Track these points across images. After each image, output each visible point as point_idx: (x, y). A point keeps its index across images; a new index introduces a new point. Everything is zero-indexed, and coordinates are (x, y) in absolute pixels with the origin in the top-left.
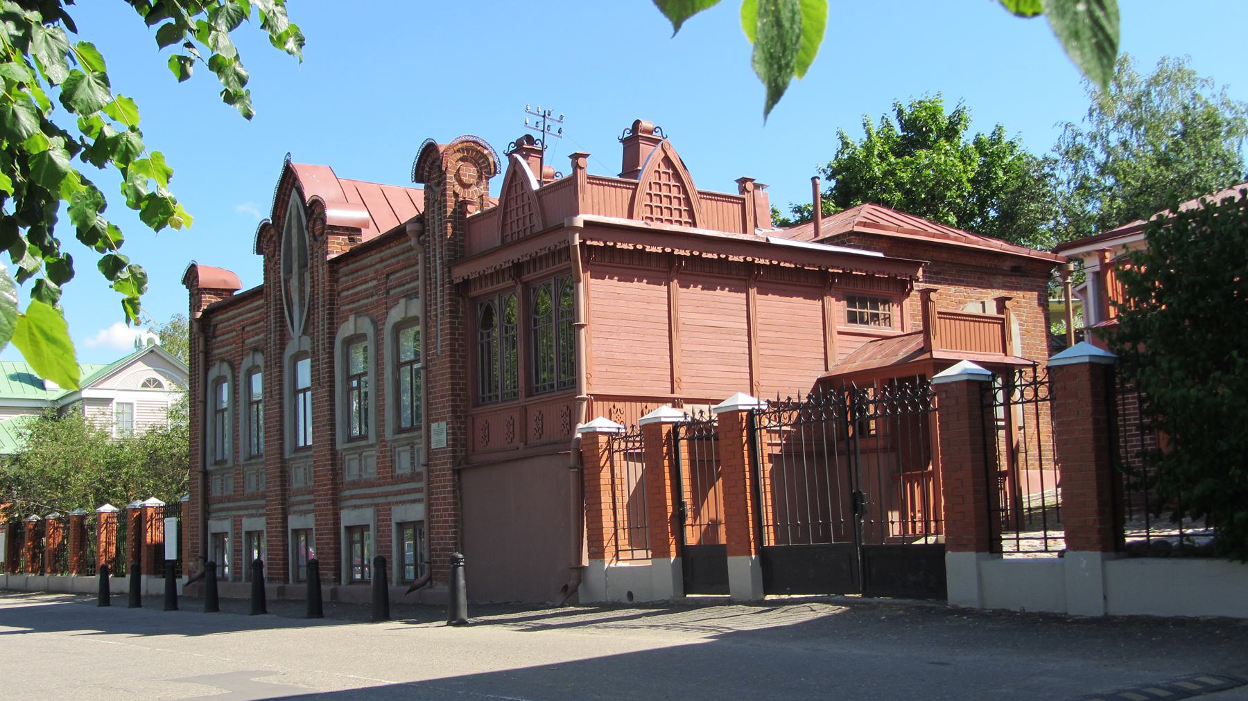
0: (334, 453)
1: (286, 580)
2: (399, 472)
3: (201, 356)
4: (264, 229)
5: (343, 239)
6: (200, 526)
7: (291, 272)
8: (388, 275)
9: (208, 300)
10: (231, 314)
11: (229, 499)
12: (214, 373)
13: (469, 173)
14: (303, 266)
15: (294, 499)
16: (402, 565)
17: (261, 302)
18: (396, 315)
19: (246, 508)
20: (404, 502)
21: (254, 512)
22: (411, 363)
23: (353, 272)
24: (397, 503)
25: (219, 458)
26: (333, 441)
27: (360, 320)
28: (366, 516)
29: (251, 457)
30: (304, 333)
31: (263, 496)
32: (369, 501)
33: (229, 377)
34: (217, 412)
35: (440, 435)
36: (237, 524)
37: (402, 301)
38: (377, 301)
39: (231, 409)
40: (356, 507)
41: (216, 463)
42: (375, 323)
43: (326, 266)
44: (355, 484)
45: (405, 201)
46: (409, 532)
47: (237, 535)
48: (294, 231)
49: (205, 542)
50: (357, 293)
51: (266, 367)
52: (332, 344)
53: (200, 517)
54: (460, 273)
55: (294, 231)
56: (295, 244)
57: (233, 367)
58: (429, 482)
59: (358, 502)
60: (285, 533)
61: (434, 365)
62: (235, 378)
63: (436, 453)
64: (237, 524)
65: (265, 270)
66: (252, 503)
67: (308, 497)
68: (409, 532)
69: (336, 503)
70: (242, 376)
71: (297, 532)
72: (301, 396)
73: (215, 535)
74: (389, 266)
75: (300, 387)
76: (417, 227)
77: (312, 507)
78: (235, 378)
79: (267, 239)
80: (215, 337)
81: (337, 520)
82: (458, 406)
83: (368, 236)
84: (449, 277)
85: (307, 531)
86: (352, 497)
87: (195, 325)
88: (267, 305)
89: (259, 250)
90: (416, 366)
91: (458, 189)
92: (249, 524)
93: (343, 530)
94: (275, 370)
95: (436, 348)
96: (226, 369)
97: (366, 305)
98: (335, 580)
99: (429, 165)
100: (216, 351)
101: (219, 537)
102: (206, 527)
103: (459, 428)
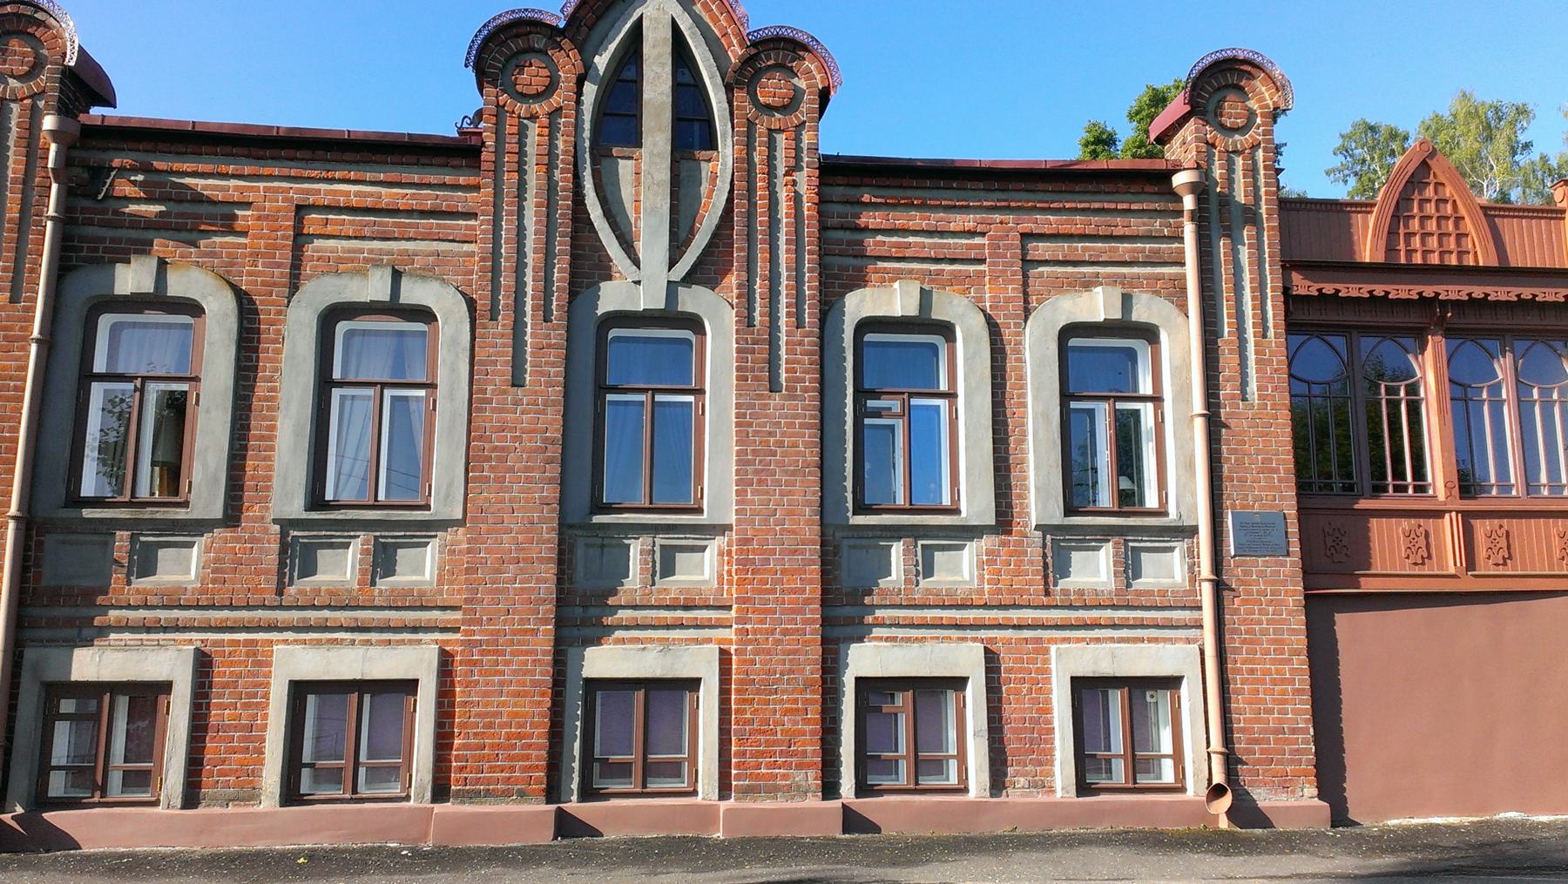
59: (900, 633)
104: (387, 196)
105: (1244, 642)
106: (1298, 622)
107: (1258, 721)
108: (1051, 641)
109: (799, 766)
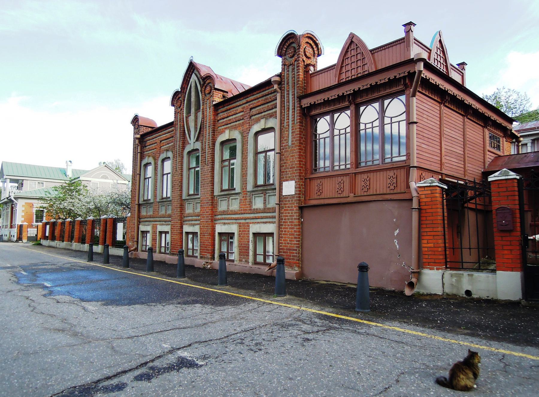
0: (213, 197)
1: (213, 258)
2: (254, 207)
3: (139, 154)
4: (176, 94)
5: (220, 94)
6: (136, 227)
7: (190, 113)
8: (161, 141)
9: (144, 130)
10: (154, 136)
11: (150, 217)
12: (144, 162)
13: (309, 51)
14: (198, 109)
15: (186, 218)
16: (255, 255)
17: (173, 128)
18: (163, 156)
19: (160, 221)
20: (258, 223)
21: (164, 223)
22: (195, 168)
23: (227, 110)
24: (253, 223)
25: (146, 198)
26: (213, 191)
27: (232, 132)
28: (233, 228)
29: (163, 199)
30: (197, 140)
31: (170, 216)
32: (234, 221)
33: (153, 163)
34: (145, 179)
35: (289, 188)
36: (154, 228)
37: (165, 152)
38: (243, 123)
39: (153, 177)
40: (225, 224)
41: (144, 201)
42: (242, 133)
43: (212, 108)
44: (224, 213)
45: (268, 66)
46: (190, 236)
47: (154, 232)
48: (193, 94)
49: (138, 235)
50: (230, 120)
51: (174, 157)
52: (214, 144)
53: (136, 224)
54: (306, 102)
55: (193, 94)
56: (193, 99)
57: (155, 159)
58: (280, 213)
59: (226, 221)
60: (182, 233)
61: (286, 151)
62: (156, 164)
63: (285, 198)
64: (154, 228)
65: (175, 114)
66: (163, 219)
67: (197, 218)
68: (190, 236)
69: (213, 221)
70: (159, 163)
71: (188, 233)
72: (165, 176)
73: (143, 232)
74: (252, 104)
75: (165, 173)
76: (278, 79)
77: (199, 222)
78: (156, 164)
79: (177, 98)
80: (146, 147)
81: (214, 229)
82: (302, 173)
83: (230, 95)
84: (300, 104)
85: (194, 234)
86: (222, 219)
87: (137, 141)
88: (176, 130)
89: (173, 105)
90: (197, 169)
91: (305, 59)
92: (160, 228)
93: (217, 234)
94: (179, 159)
95: (288, 142)
96: (151, 160)
97: (236, 125)
98: (211, 258)
99: (289, 45)
100: (145, 153)
101: (145, 233)
102: (138, 228)
103: (302, 185)
104: (258, 95)
105: (284, 222)
106: (296, 216)
107: (285, 246)
108: (250, 223)
109: (208, 253)
